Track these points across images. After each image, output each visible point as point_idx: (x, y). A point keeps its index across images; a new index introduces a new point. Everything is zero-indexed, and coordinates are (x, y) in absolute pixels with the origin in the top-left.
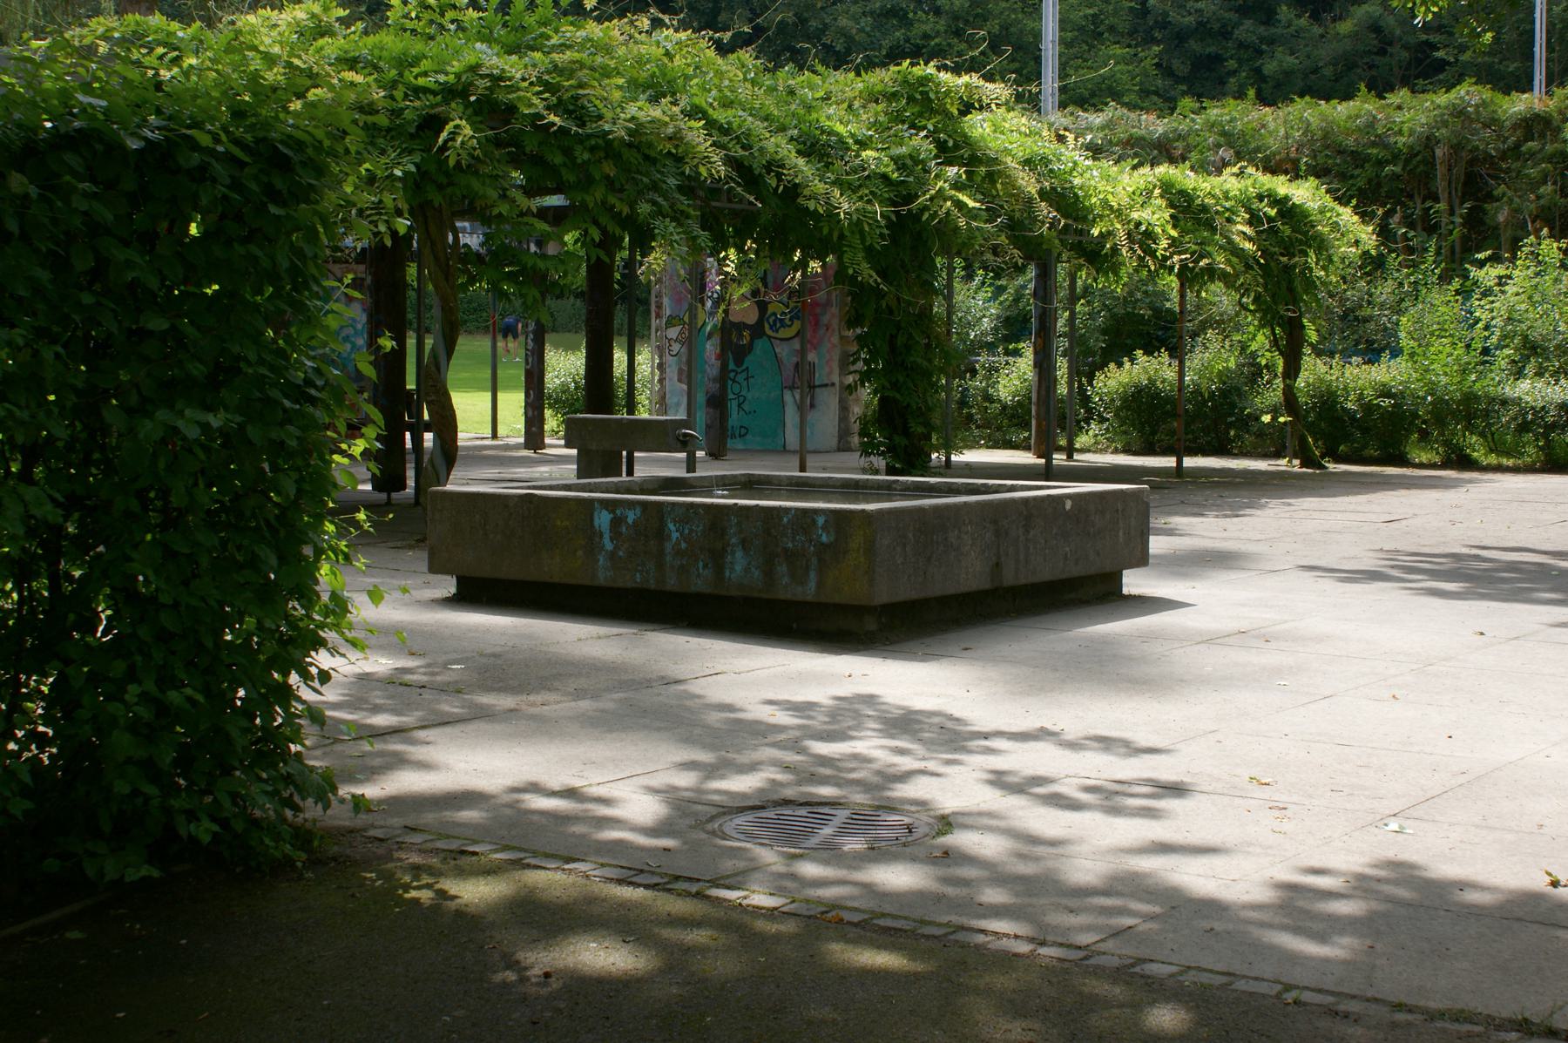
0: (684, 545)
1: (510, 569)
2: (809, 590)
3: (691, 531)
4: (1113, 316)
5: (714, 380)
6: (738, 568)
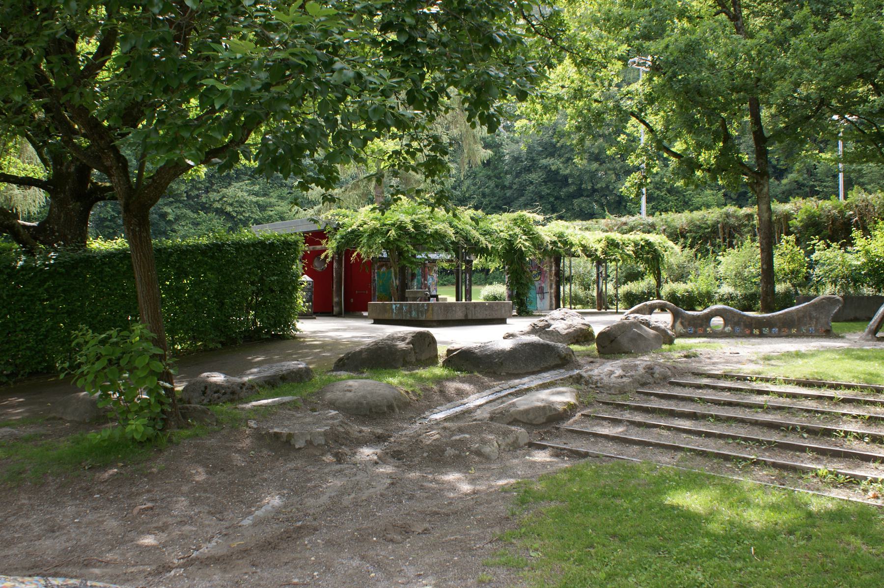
1: (380, 317)
2: (423, 318)
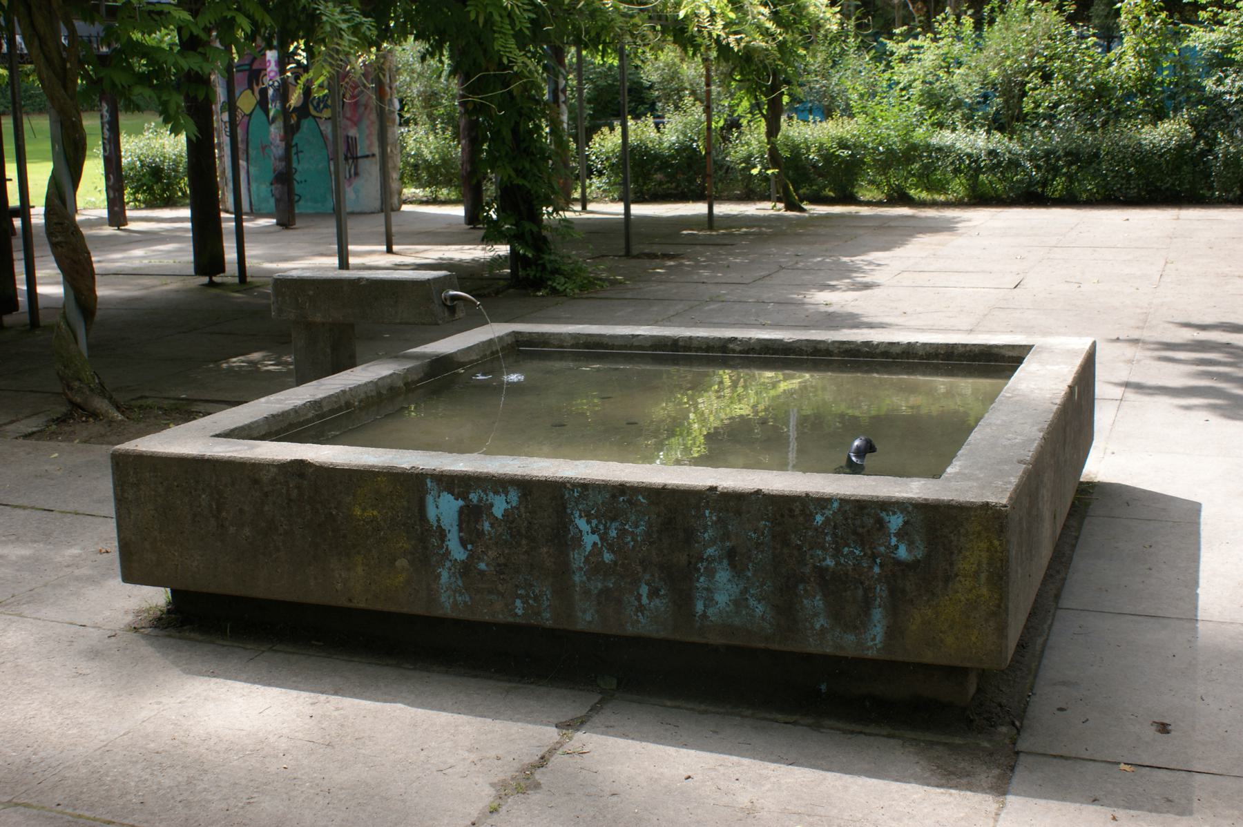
0: (608, 557)
1: (273, 582)
3: (622, 533)
4: (596, 87)
5: (281, 159)
6: (722, 599)
